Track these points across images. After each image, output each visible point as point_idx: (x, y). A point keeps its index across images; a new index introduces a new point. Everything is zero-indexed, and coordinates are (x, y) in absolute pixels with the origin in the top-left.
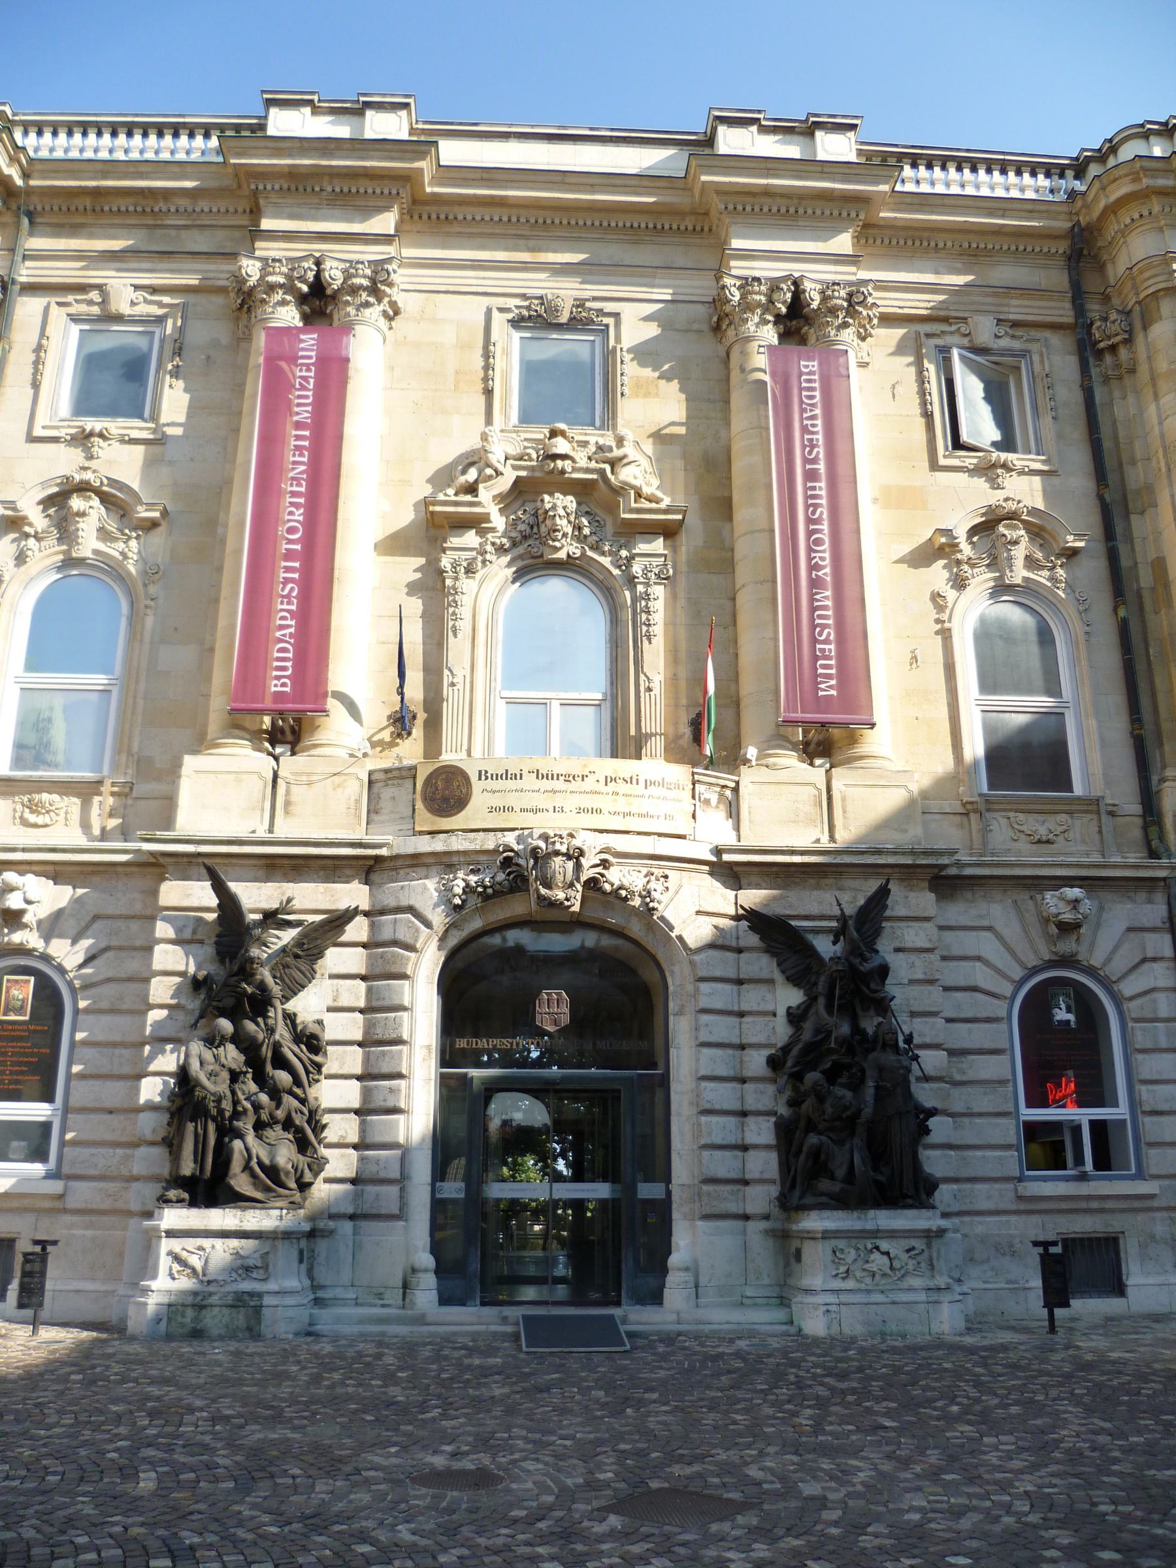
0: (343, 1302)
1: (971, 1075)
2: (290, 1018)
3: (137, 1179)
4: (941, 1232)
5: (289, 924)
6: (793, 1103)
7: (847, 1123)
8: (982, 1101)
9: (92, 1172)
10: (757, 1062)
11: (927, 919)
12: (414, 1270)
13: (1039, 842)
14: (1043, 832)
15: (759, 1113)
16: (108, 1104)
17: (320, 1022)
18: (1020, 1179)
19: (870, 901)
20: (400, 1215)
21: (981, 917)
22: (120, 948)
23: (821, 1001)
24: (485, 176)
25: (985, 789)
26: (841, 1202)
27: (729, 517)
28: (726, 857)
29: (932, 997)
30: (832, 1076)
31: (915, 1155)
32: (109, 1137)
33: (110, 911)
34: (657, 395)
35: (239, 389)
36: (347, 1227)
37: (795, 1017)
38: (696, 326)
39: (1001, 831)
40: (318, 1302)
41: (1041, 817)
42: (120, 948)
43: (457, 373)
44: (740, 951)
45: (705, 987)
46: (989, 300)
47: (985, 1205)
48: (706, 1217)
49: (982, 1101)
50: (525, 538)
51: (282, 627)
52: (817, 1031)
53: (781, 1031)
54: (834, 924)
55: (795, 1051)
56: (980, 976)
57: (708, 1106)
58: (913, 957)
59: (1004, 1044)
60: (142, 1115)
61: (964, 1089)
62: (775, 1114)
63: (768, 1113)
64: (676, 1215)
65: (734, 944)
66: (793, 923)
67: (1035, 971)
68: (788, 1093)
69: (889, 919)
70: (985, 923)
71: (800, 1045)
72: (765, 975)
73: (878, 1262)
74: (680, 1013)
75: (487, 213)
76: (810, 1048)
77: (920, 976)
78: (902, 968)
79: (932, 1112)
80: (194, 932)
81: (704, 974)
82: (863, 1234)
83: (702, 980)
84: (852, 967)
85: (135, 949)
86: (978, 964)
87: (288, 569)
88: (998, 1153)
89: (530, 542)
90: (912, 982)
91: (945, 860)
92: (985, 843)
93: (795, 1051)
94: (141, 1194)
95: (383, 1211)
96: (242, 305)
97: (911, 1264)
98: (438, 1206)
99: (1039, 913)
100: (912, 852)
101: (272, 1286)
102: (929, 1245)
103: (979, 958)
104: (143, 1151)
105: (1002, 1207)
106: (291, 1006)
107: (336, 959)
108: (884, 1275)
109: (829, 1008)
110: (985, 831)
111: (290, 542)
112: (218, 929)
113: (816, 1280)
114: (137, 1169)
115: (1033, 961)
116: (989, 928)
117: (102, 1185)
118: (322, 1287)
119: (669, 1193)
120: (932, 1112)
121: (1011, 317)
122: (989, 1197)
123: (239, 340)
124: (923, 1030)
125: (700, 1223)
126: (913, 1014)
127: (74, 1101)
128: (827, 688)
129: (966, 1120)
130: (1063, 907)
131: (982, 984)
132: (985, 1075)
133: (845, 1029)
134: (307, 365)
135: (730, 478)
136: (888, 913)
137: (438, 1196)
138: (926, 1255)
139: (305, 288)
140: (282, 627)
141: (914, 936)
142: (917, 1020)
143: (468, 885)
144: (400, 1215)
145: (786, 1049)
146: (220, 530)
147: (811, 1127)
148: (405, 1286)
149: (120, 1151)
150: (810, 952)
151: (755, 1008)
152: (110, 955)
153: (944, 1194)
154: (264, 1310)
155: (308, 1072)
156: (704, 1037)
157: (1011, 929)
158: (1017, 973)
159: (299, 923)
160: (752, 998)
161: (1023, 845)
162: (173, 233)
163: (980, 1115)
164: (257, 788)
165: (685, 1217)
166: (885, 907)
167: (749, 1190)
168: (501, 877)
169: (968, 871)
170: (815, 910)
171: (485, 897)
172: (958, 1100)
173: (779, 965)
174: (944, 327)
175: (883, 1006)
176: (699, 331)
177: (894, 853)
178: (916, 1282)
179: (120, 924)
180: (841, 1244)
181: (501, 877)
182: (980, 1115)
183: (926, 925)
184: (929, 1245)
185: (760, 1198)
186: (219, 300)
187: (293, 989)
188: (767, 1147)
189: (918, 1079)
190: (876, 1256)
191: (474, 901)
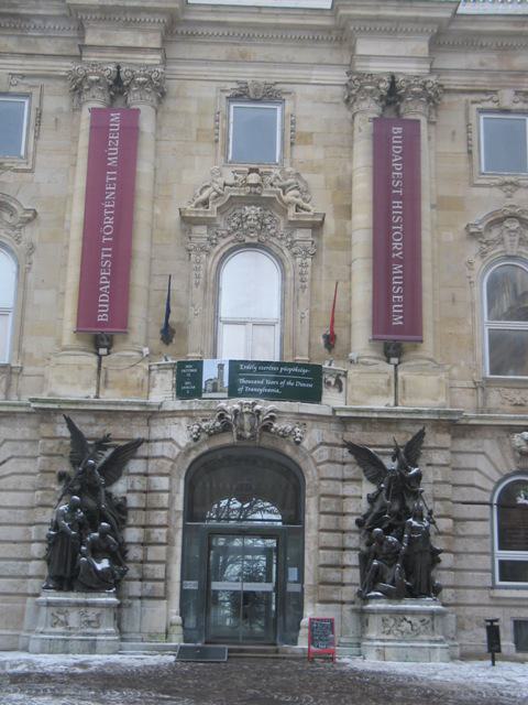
0: (136, 640)
1: (468, 532)
2: (109, 495)
3: (30, 577)
4: (441, 614)
5: (109, 447)
6: (369, 545)
7: (392, 556)
8: (474, 546)
9: (6, 573)
10: (350, 522)
11: (446, 449)
12: (171, 625)
13: (516, 405)
14: (518, 399)
15: (351, 549)
16: (14, 539)
17: (125, 498)
18: (493, 587)
19: (415, 437)
20: (165, 597)
21: (479, 447)
22: (18, 457)
23: (384, 492)
24: (215, 9)
25: (488, 375)
26: (388, 595)
27: (350, 218)
28: (338, 414)
29: (446, 491)
30: (387, 531)
31: (429, 573)
32: (14, 555)
33: (13, 437)
34: (311, 143)
35: (75, 140)
36: (138, 602)
37: (372, 500)
38: (336, 100)
39: (495, 398)
40: (122, 640)
41: (517, 391)
42: (18, 457)
43: (198, 130)
44: (344, 464)
45: (324, 483)
46: (512, 79)
47: (472, 601)
48: (321, 602)
49: (474, 546)
50: (235, 230)
51: (103, 285)
52: (382, 508)
53: (364, 506)
54: (392, 450)
55: (370, 518)
56: (477, 479)
57: (323, 545)
58: (437, 469)
59: (488, 516)
60: (33, 545)
61: (464, 540)
62: (359, 549)
63: (355, 549)
64: (305, 600)
65: (341, 460)
66: (371, 450)
67: (507, 476)
68: (367, 539)
69: (424, 448)
70: (480, 450)
71: (372, 515)
72: (357, 477)
73: (406, 625)
74: (310, 497)
75: (215, 31)
76: (379, 515)
77: (440, 479)
78: (430, 475)
79: (440, 551)
80: (58, 450)
81: (324, 476)
82: (398, 612)
83: (322, 479)
84: (402, 475)
85: (25, 457)
86: (476, 472)
87: (106, 252)
88: (480, 574)
89: (238, 232)
90: (435, 483)
91: (457, 418)
92: (485, 404)
93: (370, 518)
94: (34, 585)
95: (156, 595)
96: (76, 89)
97: (422, 628)
98: (184, 594)
99: (510, 445)
100: (438, 412)
101: (102, 630)
102: (433, 619)
103: (476, 469)
104: (33, 563)
105: (482, 601)
106: (109, 489)
107: (136, 466)
108: (408, 633)
109: (387, 495)
110: (485, 397)
111: (107, 236)
112: (71, 449)
113: (372, 635)
114: (31, 572)
115: (506, 471)
116: (483, 453)
117: (10, 580)
118: (126, 633)
119: (303, 589)
120: (440, 551)
121: (524, 89)
122: (474, 597)
123: (74, 110)
124: (438, 508)
125: (317, 605)
126: (435, 499)
127: (488, 558)
128: (397, 321)
129: (464, 556)
130: (523, 443)
131: (478, 483)
132: (476, 532)
133: (396, 507)
134: (115, 132)
135: (351, 194)
136: (424, 445)
137: (185, 588)
138: (430, 624)
139: (111, 82)
140: (103, 285)
141: (438, 458)
142: (437, 503)
143: (200, 428)
144: (165, 597)
145: (365, 516)
146: (66, 225)
147: (376, 557)
148: (167, 633)
149: (20, 563)
150: (380, 465)
151: (352, 494)
152: (13, 461)
153: (447, 594)
154: (98, 643)
155: (118, 524)
156: (322, 509)
157: (496, 454)
158: (497, 477)
159: (114, 446)
160: (349, 489)
161: (507, 407)
162: (32, 40)
163: (472, 553)
164: (90, 373)
165: (310, 601)
166: (422, 442)
167: (344, 589)
168: (218, 424)
169: (471, 422)
170: (385, 442)
171: (210, 435)
172: (460, 545)
173: (365, 471)
174: (484, 97)
175: (417, 495)
176: (338, 103)
177: (429, 412)
178: (425, 637)
179: (17, 444)
180: (387, 616)
181: (218, 424)
182: (472, 553)
183: (445, 452)
184: (433, 619)
185: (349, 593)
186: (61, 84)
187: (111, 481)
188: (356, 567)
189: (436, 534)
190: (405, 623)
191: (203, 436)
